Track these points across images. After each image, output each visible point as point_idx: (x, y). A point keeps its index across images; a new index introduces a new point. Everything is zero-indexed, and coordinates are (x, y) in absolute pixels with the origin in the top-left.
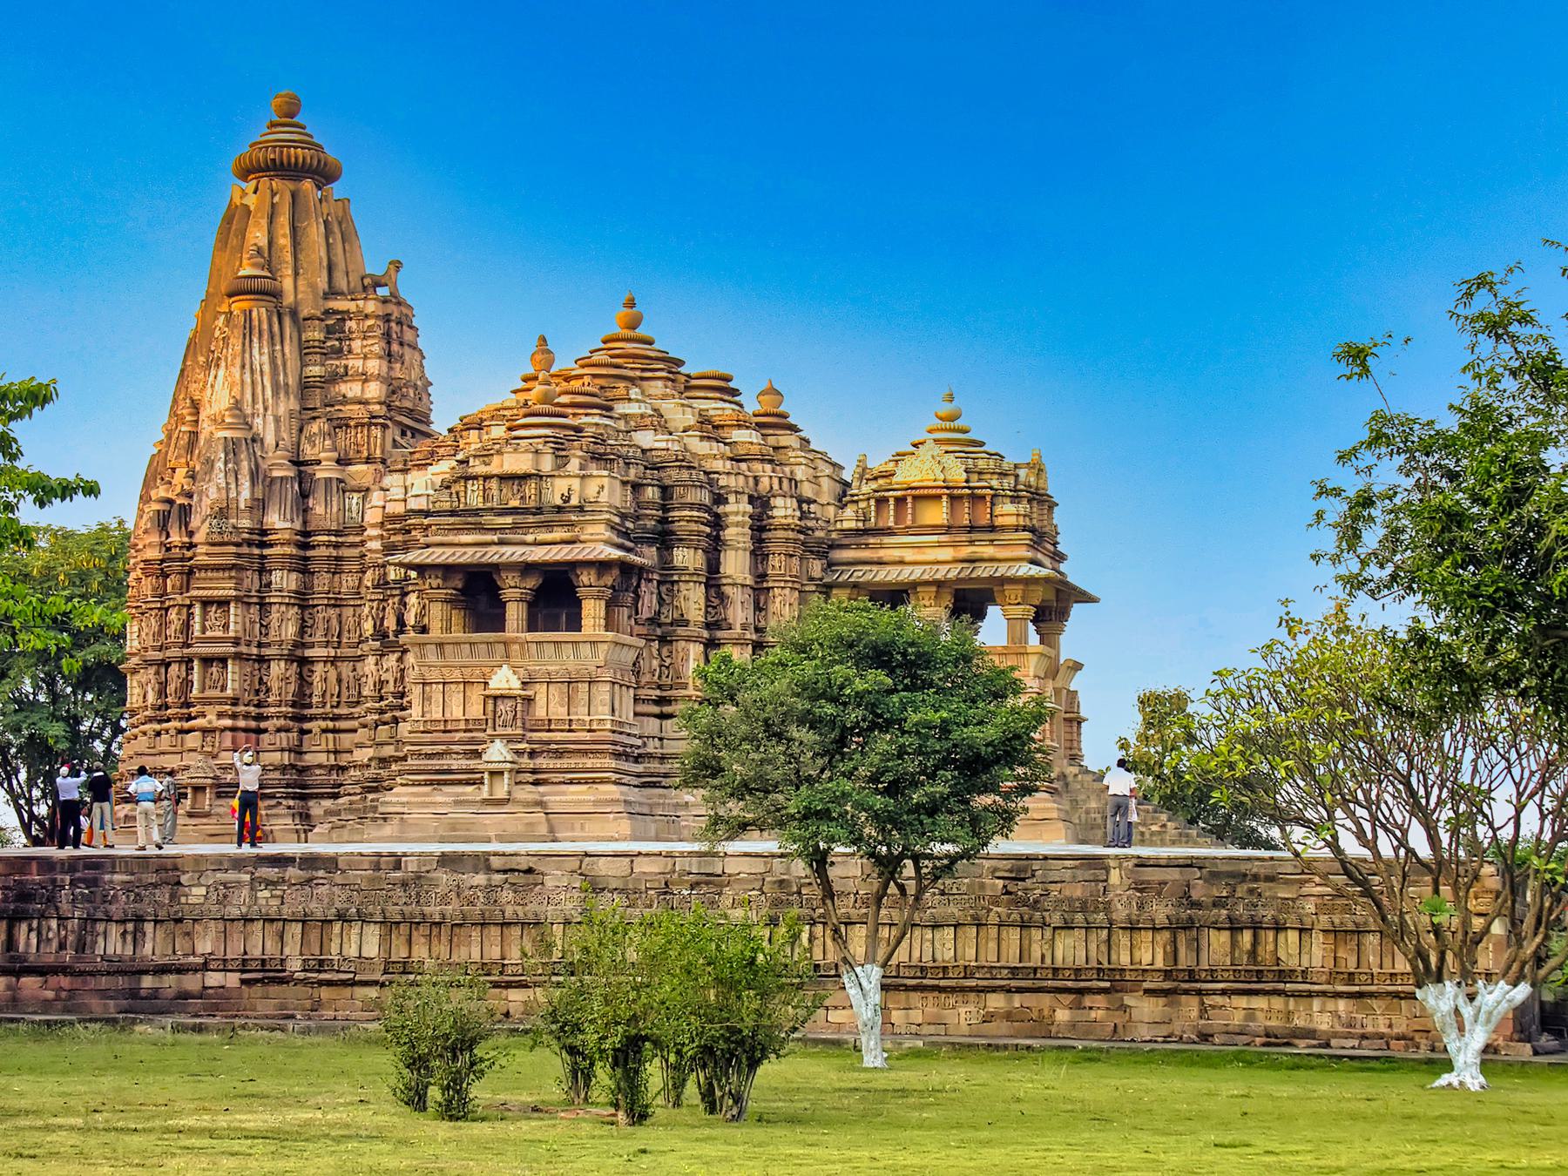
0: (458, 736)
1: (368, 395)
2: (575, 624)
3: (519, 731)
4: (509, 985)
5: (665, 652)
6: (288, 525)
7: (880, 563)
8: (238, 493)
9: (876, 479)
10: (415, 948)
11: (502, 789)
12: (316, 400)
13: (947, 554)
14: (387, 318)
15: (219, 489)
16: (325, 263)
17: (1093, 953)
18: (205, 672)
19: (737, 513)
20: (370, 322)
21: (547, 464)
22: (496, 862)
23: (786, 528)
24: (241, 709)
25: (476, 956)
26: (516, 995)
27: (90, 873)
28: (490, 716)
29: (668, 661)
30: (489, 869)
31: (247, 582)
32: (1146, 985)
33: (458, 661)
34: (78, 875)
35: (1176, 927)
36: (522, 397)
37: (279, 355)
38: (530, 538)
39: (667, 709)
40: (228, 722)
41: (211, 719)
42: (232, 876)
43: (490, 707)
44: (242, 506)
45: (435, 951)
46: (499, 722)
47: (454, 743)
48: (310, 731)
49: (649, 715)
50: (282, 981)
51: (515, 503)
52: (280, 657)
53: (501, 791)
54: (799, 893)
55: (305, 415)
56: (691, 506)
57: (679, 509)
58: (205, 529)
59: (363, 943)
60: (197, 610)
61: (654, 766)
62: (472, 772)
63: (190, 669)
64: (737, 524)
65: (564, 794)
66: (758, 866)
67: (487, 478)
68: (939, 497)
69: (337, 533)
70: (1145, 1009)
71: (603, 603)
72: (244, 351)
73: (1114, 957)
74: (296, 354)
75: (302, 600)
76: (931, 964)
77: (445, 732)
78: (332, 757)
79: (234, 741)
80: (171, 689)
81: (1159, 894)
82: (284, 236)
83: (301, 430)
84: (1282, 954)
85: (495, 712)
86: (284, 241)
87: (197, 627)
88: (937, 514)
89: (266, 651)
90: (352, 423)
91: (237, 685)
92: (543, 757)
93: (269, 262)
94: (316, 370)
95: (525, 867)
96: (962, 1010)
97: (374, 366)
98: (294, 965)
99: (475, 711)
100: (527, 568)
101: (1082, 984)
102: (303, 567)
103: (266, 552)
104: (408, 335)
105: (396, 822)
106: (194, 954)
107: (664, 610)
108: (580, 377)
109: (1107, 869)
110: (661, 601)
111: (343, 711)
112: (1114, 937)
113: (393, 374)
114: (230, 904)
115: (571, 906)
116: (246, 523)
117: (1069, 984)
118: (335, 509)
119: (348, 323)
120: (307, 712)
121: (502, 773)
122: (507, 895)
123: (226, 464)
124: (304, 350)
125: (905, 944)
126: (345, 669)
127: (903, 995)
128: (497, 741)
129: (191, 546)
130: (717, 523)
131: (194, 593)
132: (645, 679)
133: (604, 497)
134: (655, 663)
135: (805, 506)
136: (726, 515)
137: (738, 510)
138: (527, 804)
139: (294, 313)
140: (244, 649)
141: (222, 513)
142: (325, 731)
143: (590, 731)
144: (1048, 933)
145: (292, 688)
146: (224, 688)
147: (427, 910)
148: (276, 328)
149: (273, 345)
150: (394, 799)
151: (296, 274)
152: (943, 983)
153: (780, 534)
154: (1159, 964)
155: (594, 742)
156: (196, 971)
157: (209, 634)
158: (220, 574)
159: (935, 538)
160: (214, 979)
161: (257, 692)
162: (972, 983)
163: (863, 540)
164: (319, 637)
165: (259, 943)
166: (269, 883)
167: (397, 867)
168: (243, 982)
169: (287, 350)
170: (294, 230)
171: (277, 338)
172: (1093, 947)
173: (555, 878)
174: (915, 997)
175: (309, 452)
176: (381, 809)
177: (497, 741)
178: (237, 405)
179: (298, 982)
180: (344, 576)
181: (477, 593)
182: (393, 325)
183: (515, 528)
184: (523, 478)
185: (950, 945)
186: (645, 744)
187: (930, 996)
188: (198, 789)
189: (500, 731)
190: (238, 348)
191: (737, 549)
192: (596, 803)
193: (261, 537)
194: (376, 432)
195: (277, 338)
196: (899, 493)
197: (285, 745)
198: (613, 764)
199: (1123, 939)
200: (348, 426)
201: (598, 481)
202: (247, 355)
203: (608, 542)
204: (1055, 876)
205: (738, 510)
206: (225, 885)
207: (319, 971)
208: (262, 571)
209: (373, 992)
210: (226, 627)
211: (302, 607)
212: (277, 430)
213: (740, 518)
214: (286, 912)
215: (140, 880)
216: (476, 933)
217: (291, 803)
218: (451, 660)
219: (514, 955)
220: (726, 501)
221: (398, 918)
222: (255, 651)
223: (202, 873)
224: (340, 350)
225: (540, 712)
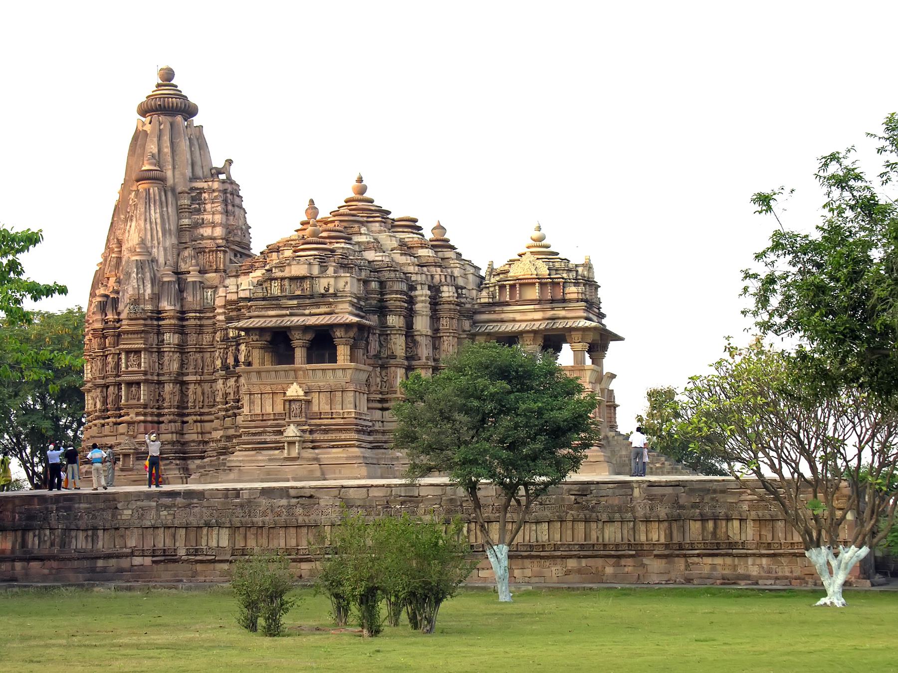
0: (270, 423)
1: (215, 235)
2: (334, 360)
3: (304, 419)
4: (301, 561)
5: (384, 373)
6: (173, 308)
7: (502, 321)
8: (145, 291)
9: (498, 274)
10: (249, 541)
11: (295, 452)
13: (539, 315)
15: (134, 289)
16: (190, 162)
17: (625, 536)
19: (422, 296)
20: (216, 194)
21: (316, 271)
22: (292, 492)
23: (449, 303)
25: (282, 545)
26: (305, 566)
27: (67, 504)
28: (287, 411)
30: (289, 496)
31: (150, 340)
32: (655, 552)
33: (269, 381)
34: (60, 505)
35: (671, 520)
36: (301, 233)
37: (165, 214)
38: (307, 312)
39: (386, 405)
40: (142, 418)
41: (132, 416)
42: (145, 503)
43: (287, 406)
44: (147, 298)
47: (268, 427)
48: (187, 422)
50: (175, 561)
51: (298, 293)
52: (170, 381)
53: (295, 452)
54: (461, 505)
55: (181, 246)
56: (397, 292)
57: (390, 294)
58: (126, 311)
59: (221, 539)
60: (123, 356)
61: (379, 437)
63: (120, 389)
64: (422, 302)
67: (282, 279)
68: (534, 284)
69: (200, 312)
70: (655, 565)
71: (349, 347)
72: (146, 212)
73: (637, 537)
75: (181, 349)
76: (535, 543)
79: (145, 428)
80: (110, 400)
81: (661, 501)
82: (167, 147)
83: (178, 255)
84: (730, 534)
85: (290, 409)
86: (167, 150)
87: (123, 365)
88: (533, 293)
90: (207, 250)
92: (317, 434)
93: (159, 162)
94: (186, 221)
95: (308, 495)
96: (553, 569)
97: (218, 218)
98: (182, 552)
99: (279, 408)
100: (306, 328)
101: (620, 553)
102: (181, 330)
103: (161, 323)
108: (333, 221)
109: (632, 489)
110: (381, 345)
111: (206, 410)
112: (637, 526)
115: (334, 515)
116: (149, 307)
117: (613, 553)
118: (198, 298)
122: (299, 511)
124: (180, 210)
125: (521, 533)
126: (206, 387)
127: (520, 561)
129: (119, 320)
130: (411, 301)
131: (121, 346)
132: (373, 389)
134: (378, 380)
135: (460, 291)
137: (422, 294)
138: (309, 459)
139: (173, 190)
140: (149, 377)
141: (136, 302)
144: (600, 525)
145: (177, 398)
146: (139, 399)
147: (255, 520)
148: (163, 198)
149: (162, 208)
150: (235, 459)
151: (174, 168)
152: (542, 554)
153: (446, 306)
154: (662, 540)
156: (127, 556)
157: (130, 369)
158: (133, 336)
159: (532, 307)
160: (137, 561)
162: (559, 553)
163: (492, 309)
164: (191, 369)
165: (162, 540)
168: (153, 562)
170: (172, 143)
171: (164, 204)
172: (625, 532)
173: (325, 500)
174: (527, 562)
175: (183, 267)
176: (228, 464)
178: (143, 242)
180: (204, 335)
181: (278, 343)
182: (228, 195)
183: (299, 306)
184: (302, 278)
185: (546, 532)
186: (374, 425)
187: (535, 561)
188: (126, 456)
189: (293, 419)
191: (422, 315)
192: (347, 458)
193: (158, 314)
194: (221, 255)
196: (511, 282)
197: (173, 430)
199: (642, 527)
200: (205, 252)
201: (344, 279)
203: (351, 313)
204: (603, 493)
205: (422, 294)
206: (142, 508)
207: (195, 555)
208: (159, 333)
209: (225, 566)
210: (139, 365)
212: (165, 255)
213: (423, 298)
214: (177, 523)
215: (95, 507)
216: (282, 532)
217: (178, 462)
218: (265, 381)
219: (304, 545)
220: (416, 289)
222: (156, 378)
223: (129, 502)
224: (199, 210)
225: (315, 409)
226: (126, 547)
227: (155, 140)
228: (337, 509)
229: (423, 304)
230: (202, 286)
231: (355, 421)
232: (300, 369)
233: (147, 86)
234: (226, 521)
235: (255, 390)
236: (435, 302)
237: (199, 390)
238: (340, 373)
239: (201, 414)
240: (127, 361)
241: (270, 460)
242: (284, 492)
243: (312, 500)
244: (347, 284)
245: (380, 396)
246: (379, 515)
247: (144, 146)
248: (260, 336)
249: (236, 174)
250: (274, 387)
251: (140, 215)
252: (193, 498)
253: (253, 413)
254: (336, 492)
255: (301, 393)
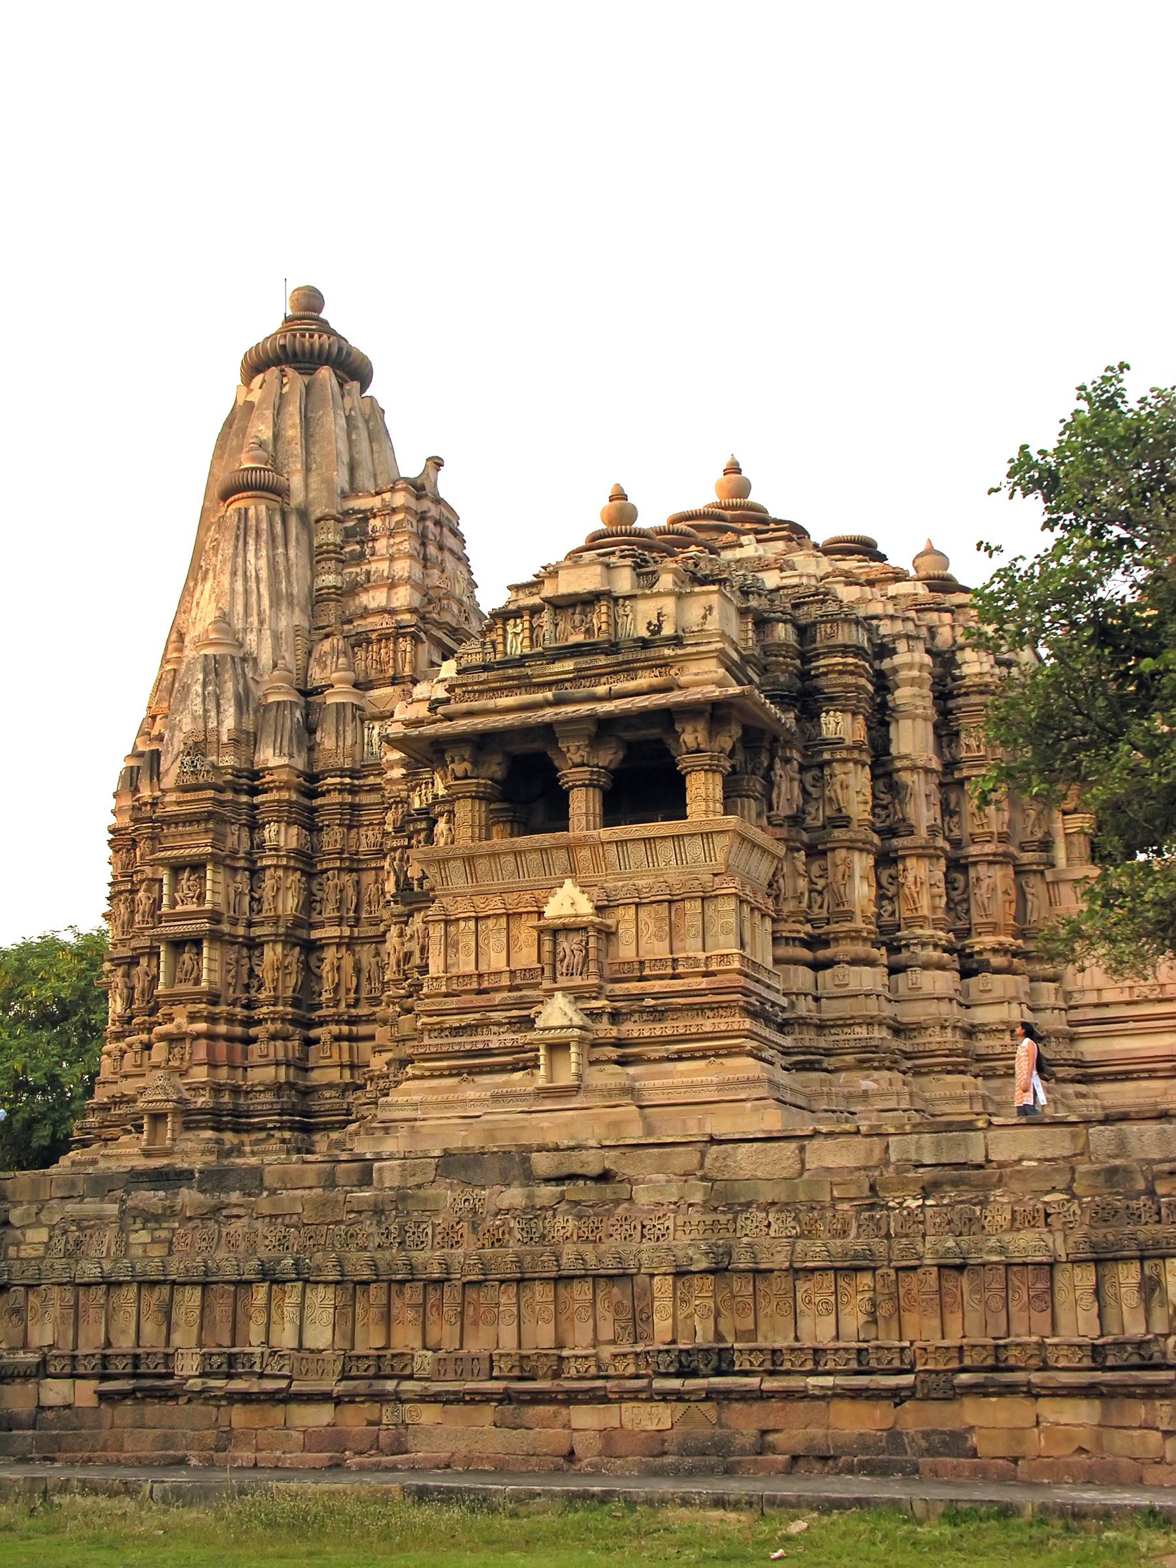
0: (498, 997)
1: (395, 604)
2: (676, 807)
3: (593, 980)
4: (571, 1398)
5: (815, 870)
6: (285, 761)
8: (220, 723)
10: (398, 1333)
11: (567, 1071)
12: (330, 615)
14: (422, 517)
15: (194, 718)
16: (345, 458)
18: (176, 961)
20: (399, 517)
21: (624, 582)
22: (542, 1163)
23: (984, 689)
24: (222, 1008)
25: (509, 1343)
26: (585, 1417)
28: (547, 957)
29: (821, 883)
30: (529, 1177)
31: (231, 841)
33: (497, 884)
37: (281, 560)
38: (601, 690)
39: (823, 954)
40: (202, 1026)
41: (180, 1022)
42: (90, 1207)
43: (547, 946)
44: (224, 739)
45: (434, 1335)
46: (561, 968)
47: (494, 1008)
48: (316, 1041)
49: (796, 962)
51: (579, 638)
52: (275, 939)
53: (566, 1076)
54: (1151, 1192)
55: (317, 631)
57: (826, 655)
58: (175, 770)
59: (308, 1324)
61: (809, 1038)
62: (521, 1049)
64: (912, 682)
65: (667, 1075)
66: (1059, 1144)
69: (354, 774)
71: (719, 779)
72: (235, 555)
74: (305, 561)
75: (307, 863)
77: (480, 992)
78: (347, 1072)
79: (210, 1051)
82: (293, 426)
83: (310, 653)
85: (554, 953)
86: (293, 431)
89: (256, 931)
90: (374, 636)
91: (216, 977)
92: (631, 1021)
93: (274, 458)
94: (330, 579)
95: (595, 1169)
97: (402, 567)
98: (188, 1366)
99: (526, 957)
100: (603, 728)
102: (309, 821)
104: (450, 541)
105: (403, 1132)
106: (25, 1346)
107: (811, 809)
111: (363, 1010)
113: (428, 582)
114: (86, 1256)
115: (688, 1242)
116: (228, 760)
118: (349, 742)
119: (372, 522)
120: (314, 1015)
121: (567, 1046)
122: (564, 1224)
123: (204, 686)
124: (317, 556)
126: (366, 954)
128: (558, 994)
130: (883, 683)
132: (788, 907)
133: (713, 624)
134: (802, 884)
136: (895, 670)
137: (911, 660)
138: (608, 1092)
139: (303, 514)
140: (226, 928)
141: (197, 748)
142: (338, 1038)
143: (705, 975)
145: (292, 981)
146: (197, 981)
147: (419, 1256)
148: (279, 528)
149: (274, 548)
150: (401, 1099)
151: (307, 470)
155: (715, 991)
156: (26, 1377)
157: (179, 908)
158: (195, 828)
160: (55, 1391)
161: (247, 987)
164: (329, 911)
165: (129, 1327)
166: (151, 1218)
167: (365, 1179)
168: (103, 1396)
169: (292, 553)
170: (306, 421)
171: (280, 541)
173: (653, 1186)
175: (317, 676)
176: (381, 1115)
177: (558, 994)
178: (224, 618)
179: (203, 1395)
180: (363, 831)
182: (430, 524)
183: (579, 676)
186: (793, 1005)
188: (158, 1118)
189: (563, 981)
190: (229, 551)
191: (914, 718)
192: (722, 1086)
193: (251, 780)
194: (405, 645)
195: (280, 541)
197: (281, 1055)
198: (748, 1024)
200: (369, 642)
201: (703, 600)
202: (240, 560)
205: (911, 660)
206: (77, 1221)
207: (229, 1376)
208: (254, 826)
209: (323, 1415)
210: (201, 898)
211: (310, 875)
212: (276, 647)
213: (915, 673)
216: (507, 1298)
217: (287, 1135)
218: (486, 883)
219: (580, 1341)
220: (894, 652)
221: (366, 1274)
222: (241, 931)
223: (42, 1205)
224: (362, 555)
225: (626, 951)
226: (25, 1346)
227: (269, 413)
228: (695, 1216)
229: (915, 690)
230: (361, 716)
231: (742, 981)
232: (582, 843)
233: (266, 321)
234: (324, 1261)
235: (461, 908)
236: (946, 688)
237: (348, 963)
238: (694, 848)
239: (353, 1021)
240: (174, 888)
241: (497, 1098)
242: (516, 1164)
243: (608, 1190)
244: (710, 615)
245: (808, 928)
246: (845, 1233)
247: (243, 431)
248: (475, 764)
249: (447, 486)
250: (511, 899)
251: (223, 562)
252: (228, 1190)
253: (454, 971)
254: (686, 1158)
255: (585, 907)
